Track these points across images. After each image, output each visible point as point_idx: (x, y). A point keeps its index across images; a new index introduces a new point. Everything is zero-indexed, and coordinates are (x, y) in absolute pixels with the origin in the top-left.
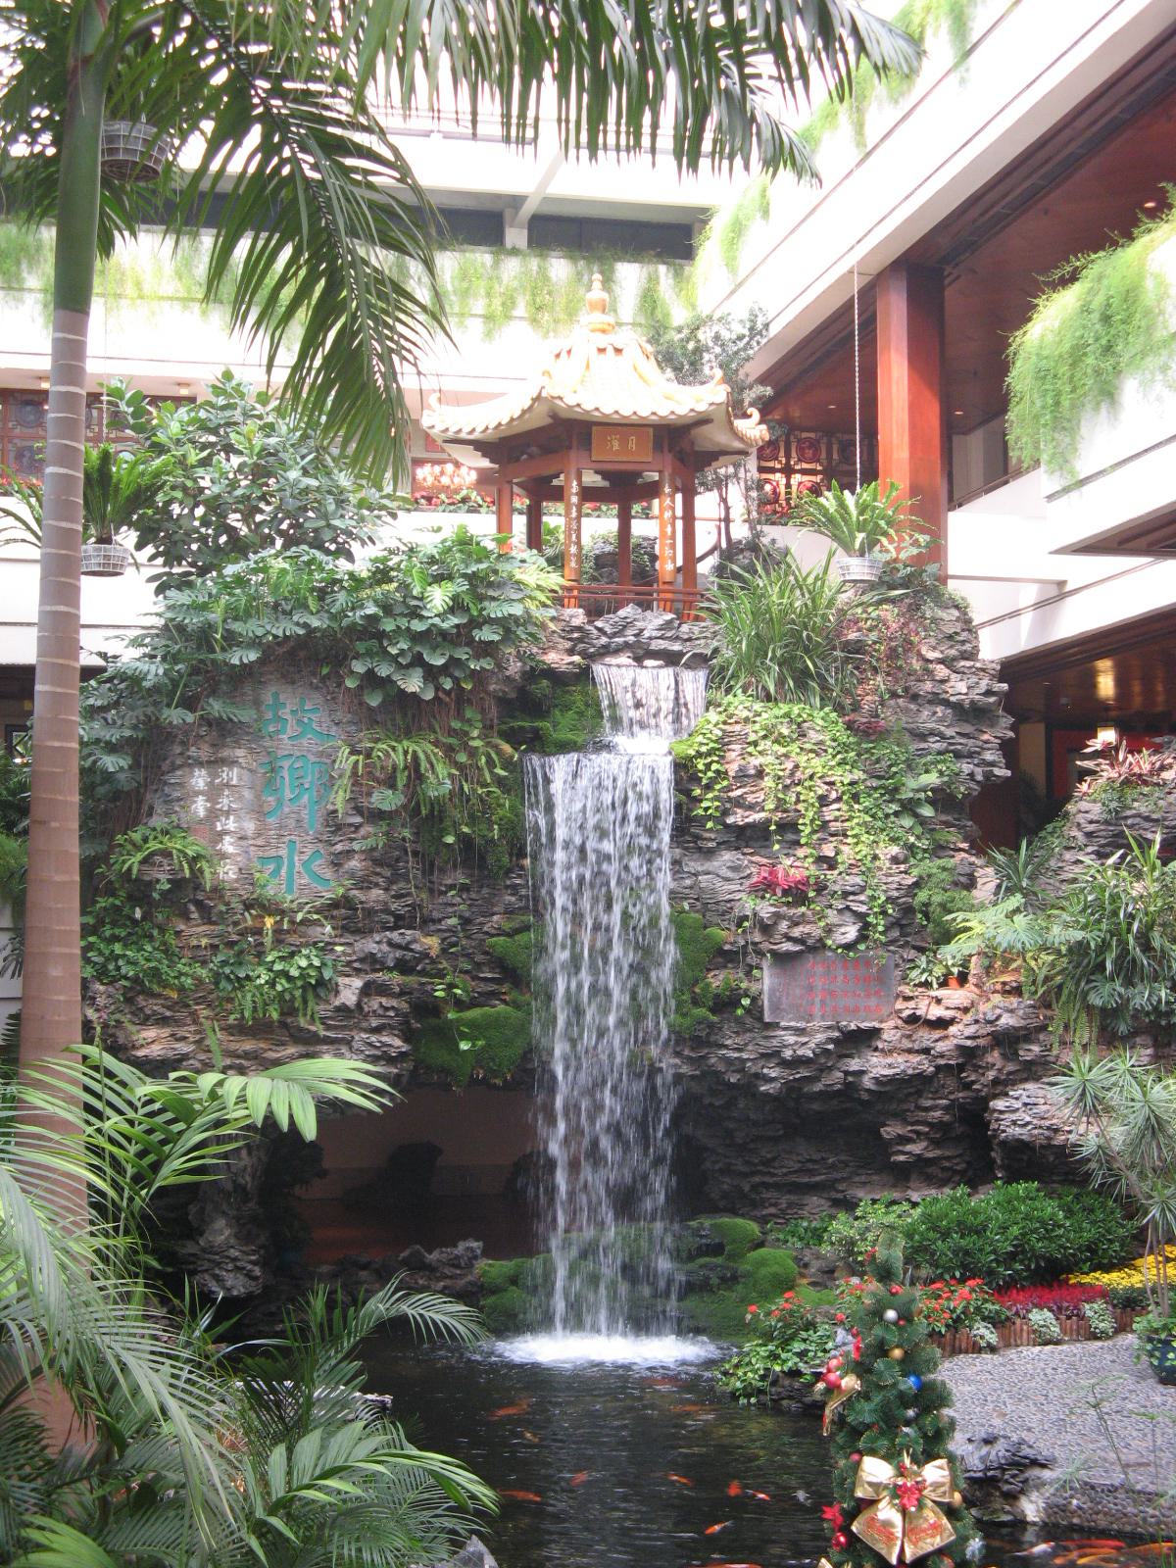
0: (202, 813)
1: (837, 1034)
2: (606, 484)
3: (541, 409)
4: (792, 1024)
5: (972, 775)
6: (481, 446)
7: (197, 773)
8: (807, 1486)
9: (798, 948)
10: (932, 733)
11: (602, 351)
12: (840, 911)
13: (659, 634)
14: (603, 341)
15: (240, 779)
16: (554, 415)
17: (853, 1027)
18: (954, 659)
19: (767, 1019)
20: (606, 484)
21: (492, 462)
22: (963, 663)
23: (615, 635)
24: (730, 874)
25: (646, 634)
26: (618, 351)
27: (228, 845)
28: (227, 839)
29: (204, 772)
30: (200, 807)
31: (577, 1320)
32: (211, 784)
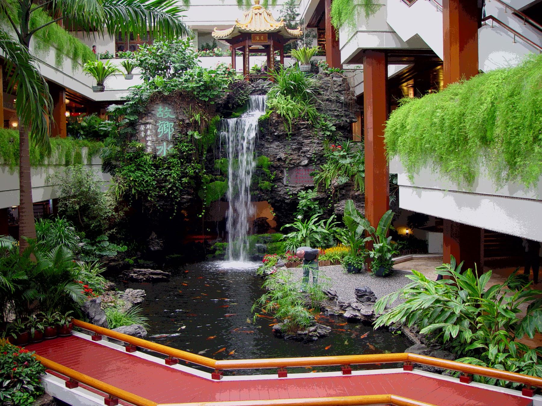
0: (143, 136)
1: (303, 188)
2: (264, 48)
3: (236, 31)
4: (292, 185)
5: (346, 121)
6: (227, 40)
7: (142, 126)
8: (165, 307)
9: (293, 166)
10: (335, 110)
11: (256, 14)
12: (303, 156)
13: (268, 86)
14: (256, 12)
15: (152, 127)
16: (240, 32)
17: (307, 186)
18: (341, 91)
19: (285, 184)
20: (264, 48)
21: (508, 19)
22: (343, 92)
23: (257, 87)
24: (276, 148)
25: (264, 87)
26: (260, 14)
27: (149, 143)
28: (149, 142)
29: (143, 126)
30: (143, 134)
31: (236, 256)
32: (145, 129)
